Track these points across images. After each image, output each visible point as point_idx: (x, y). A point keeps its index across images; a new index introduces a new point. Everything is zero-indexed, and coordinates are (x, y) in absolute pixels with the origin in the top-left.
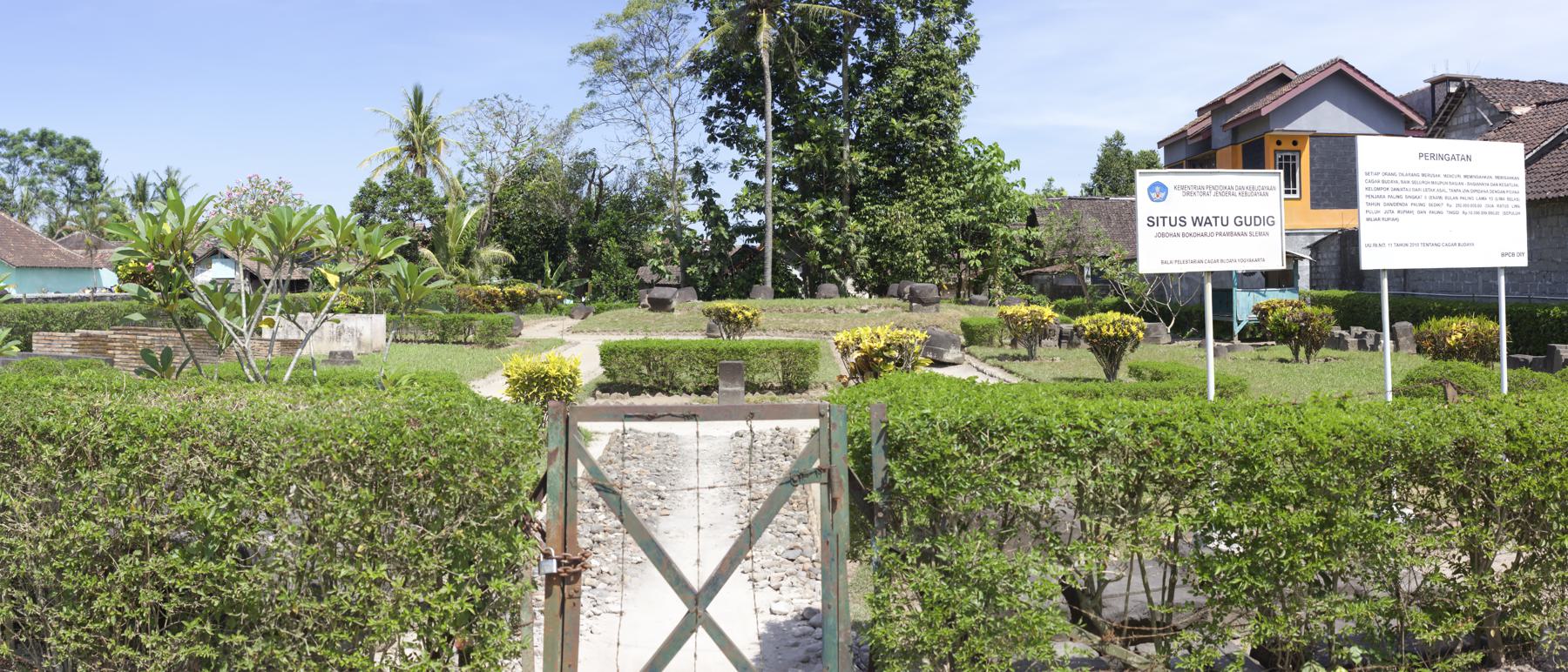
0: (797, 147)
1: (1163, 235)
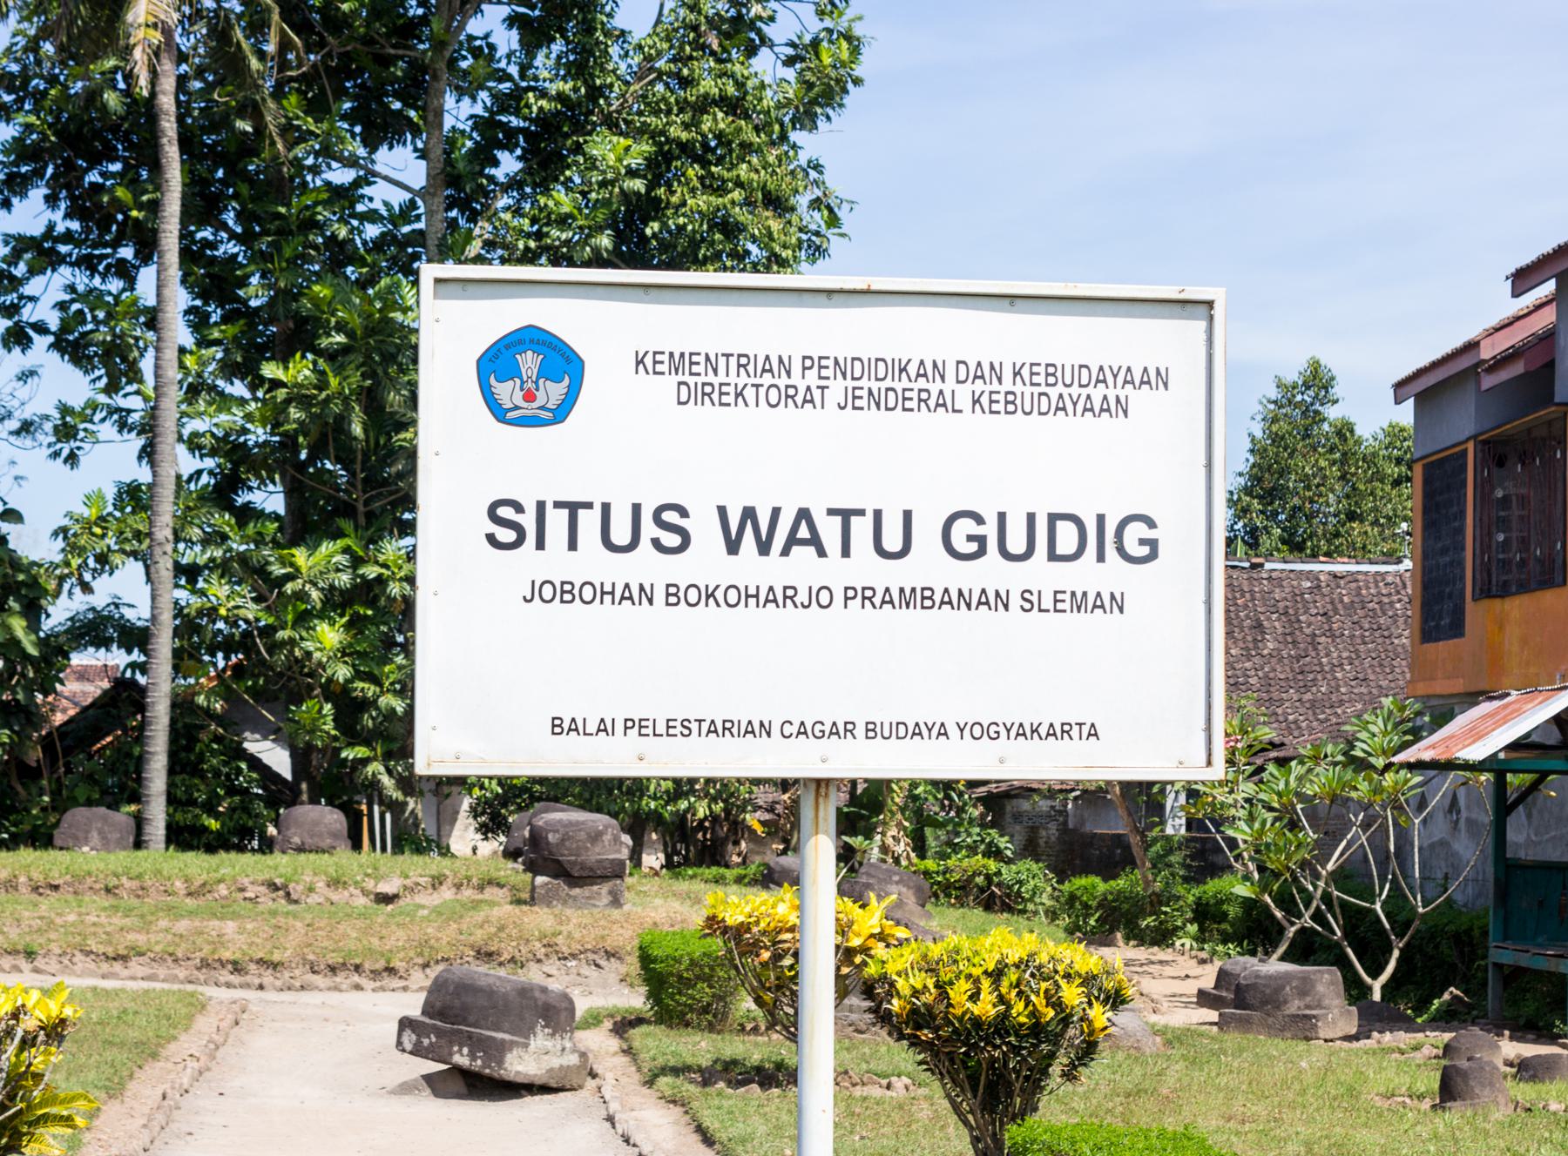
0: (270, 370)
1: (566, 592)
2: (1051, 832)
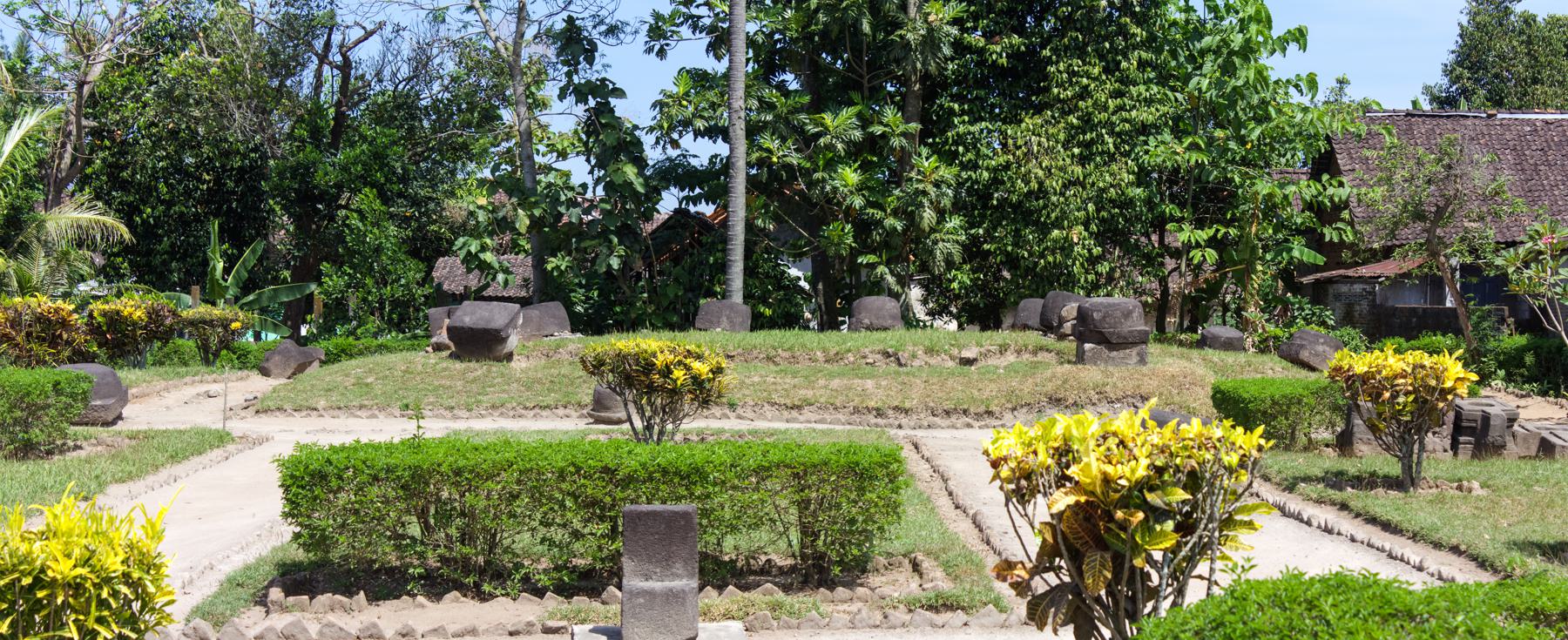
2: (1363, 307)
